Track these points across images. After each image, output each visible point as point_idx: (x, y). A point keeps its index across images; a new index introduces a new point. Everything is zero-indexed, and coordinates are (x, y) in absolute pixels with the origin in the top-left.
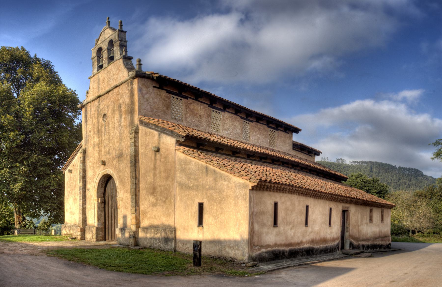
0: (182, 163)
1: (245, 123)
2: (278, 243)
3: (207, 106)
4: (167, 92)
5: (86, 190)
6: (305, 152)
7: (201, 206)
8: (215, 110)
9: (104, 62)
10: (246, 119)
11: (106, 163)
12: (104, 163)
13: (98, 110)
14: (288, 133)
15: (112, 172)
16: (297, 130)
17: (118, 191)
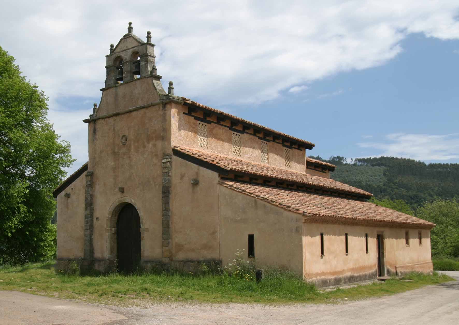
0: (227, 197)
1: (263, 144)
2: (325, 272)
3: (228, 129)
4: (194, 119)
5: (93, 219)
6: (319, 170)
7: (251, 238)
8: (235, 133)
9: (124, 75)
10: (264, 139)
11: (125, 191)
12: (122, 190)
13: (114, 130)
14: (302, 150)
15: (133, 201)
16: (310, 146)
17: (142, 222)
